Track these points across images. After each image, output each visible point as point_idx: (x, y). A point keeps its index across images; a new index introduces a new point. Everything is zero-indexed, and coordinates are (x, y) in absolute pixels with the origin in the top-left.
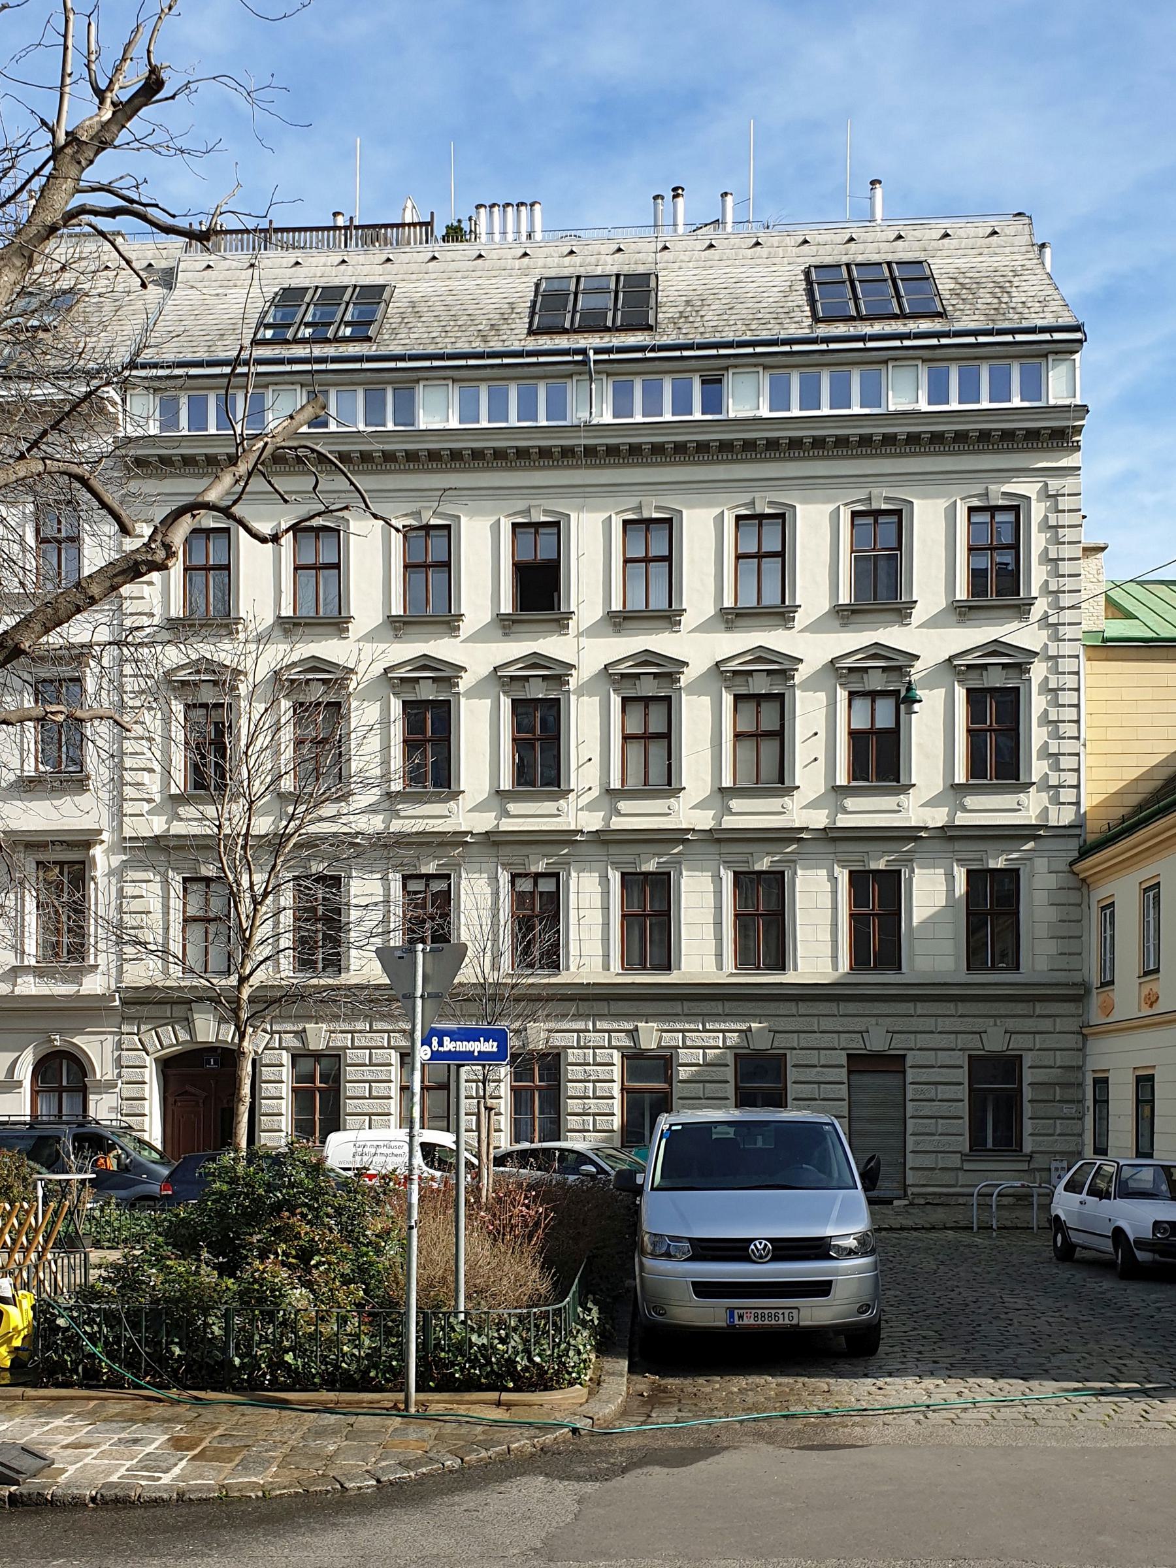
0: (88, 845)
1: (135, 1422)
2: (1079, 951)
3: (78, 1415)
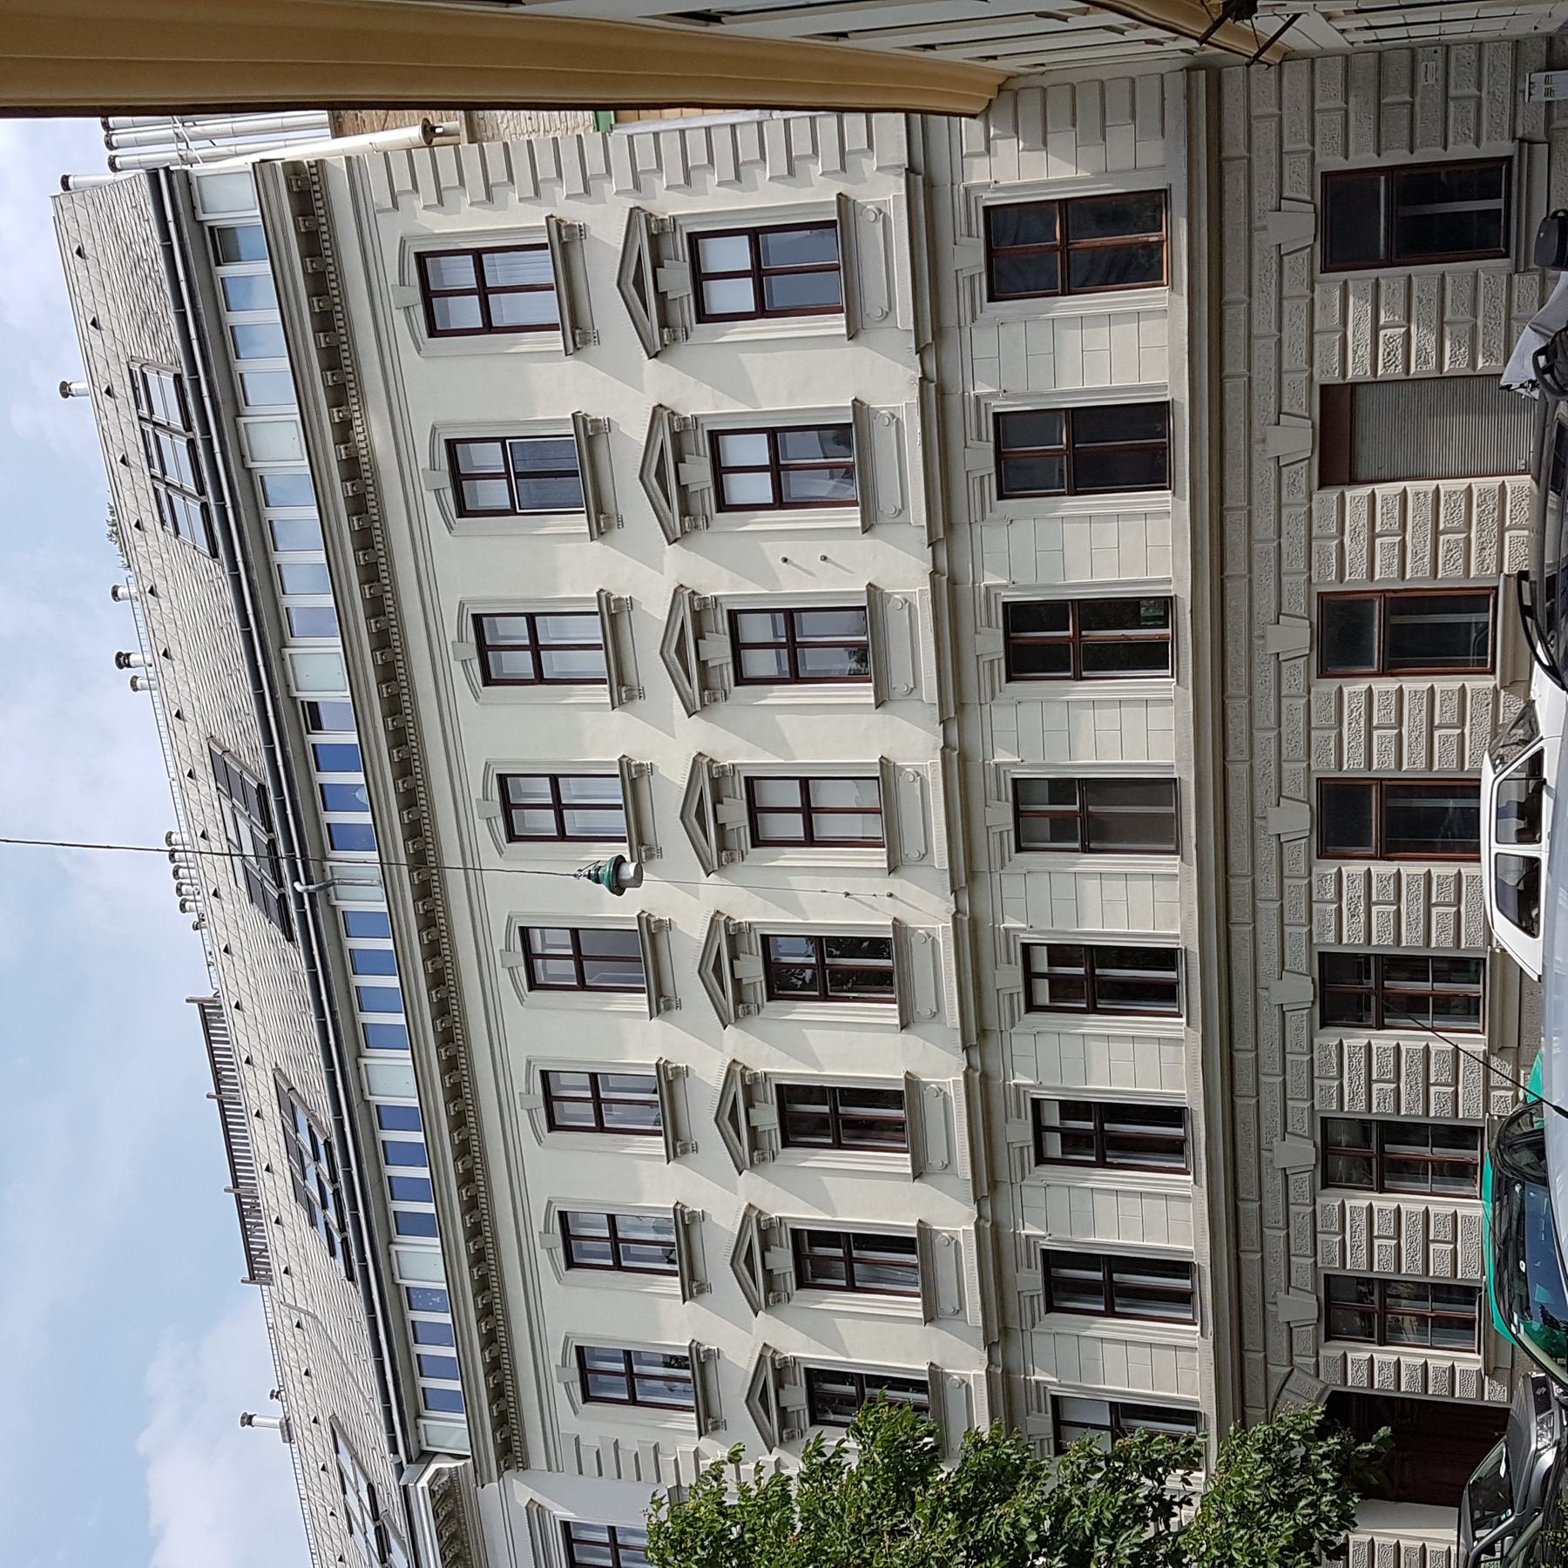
2: (1127, 83)
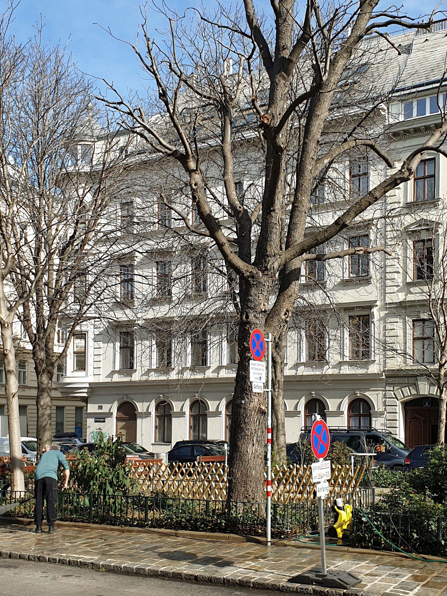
0: (371, 307)
1: (396, 566)
3: (371, 561)
